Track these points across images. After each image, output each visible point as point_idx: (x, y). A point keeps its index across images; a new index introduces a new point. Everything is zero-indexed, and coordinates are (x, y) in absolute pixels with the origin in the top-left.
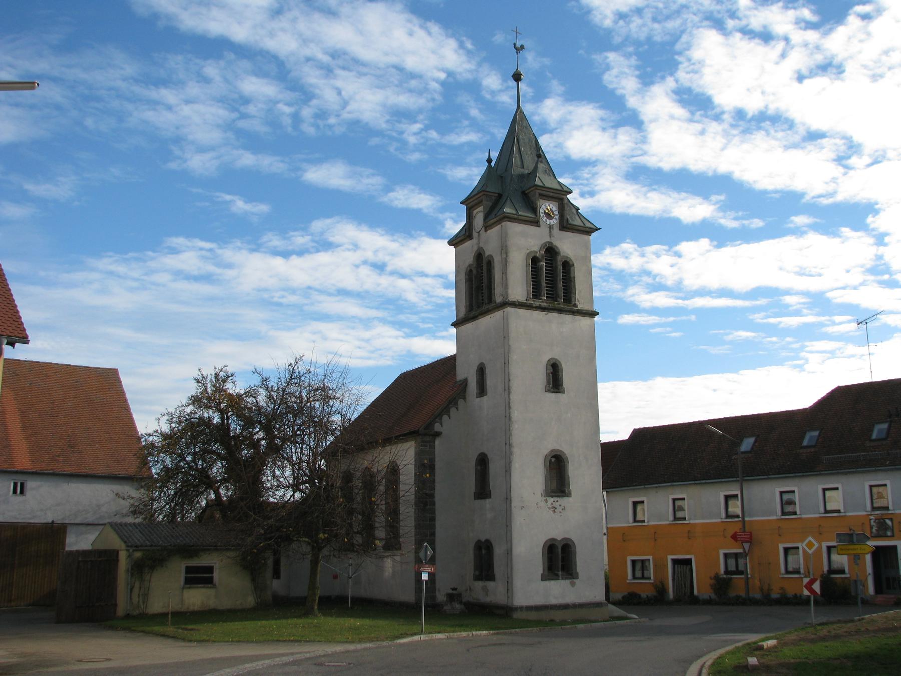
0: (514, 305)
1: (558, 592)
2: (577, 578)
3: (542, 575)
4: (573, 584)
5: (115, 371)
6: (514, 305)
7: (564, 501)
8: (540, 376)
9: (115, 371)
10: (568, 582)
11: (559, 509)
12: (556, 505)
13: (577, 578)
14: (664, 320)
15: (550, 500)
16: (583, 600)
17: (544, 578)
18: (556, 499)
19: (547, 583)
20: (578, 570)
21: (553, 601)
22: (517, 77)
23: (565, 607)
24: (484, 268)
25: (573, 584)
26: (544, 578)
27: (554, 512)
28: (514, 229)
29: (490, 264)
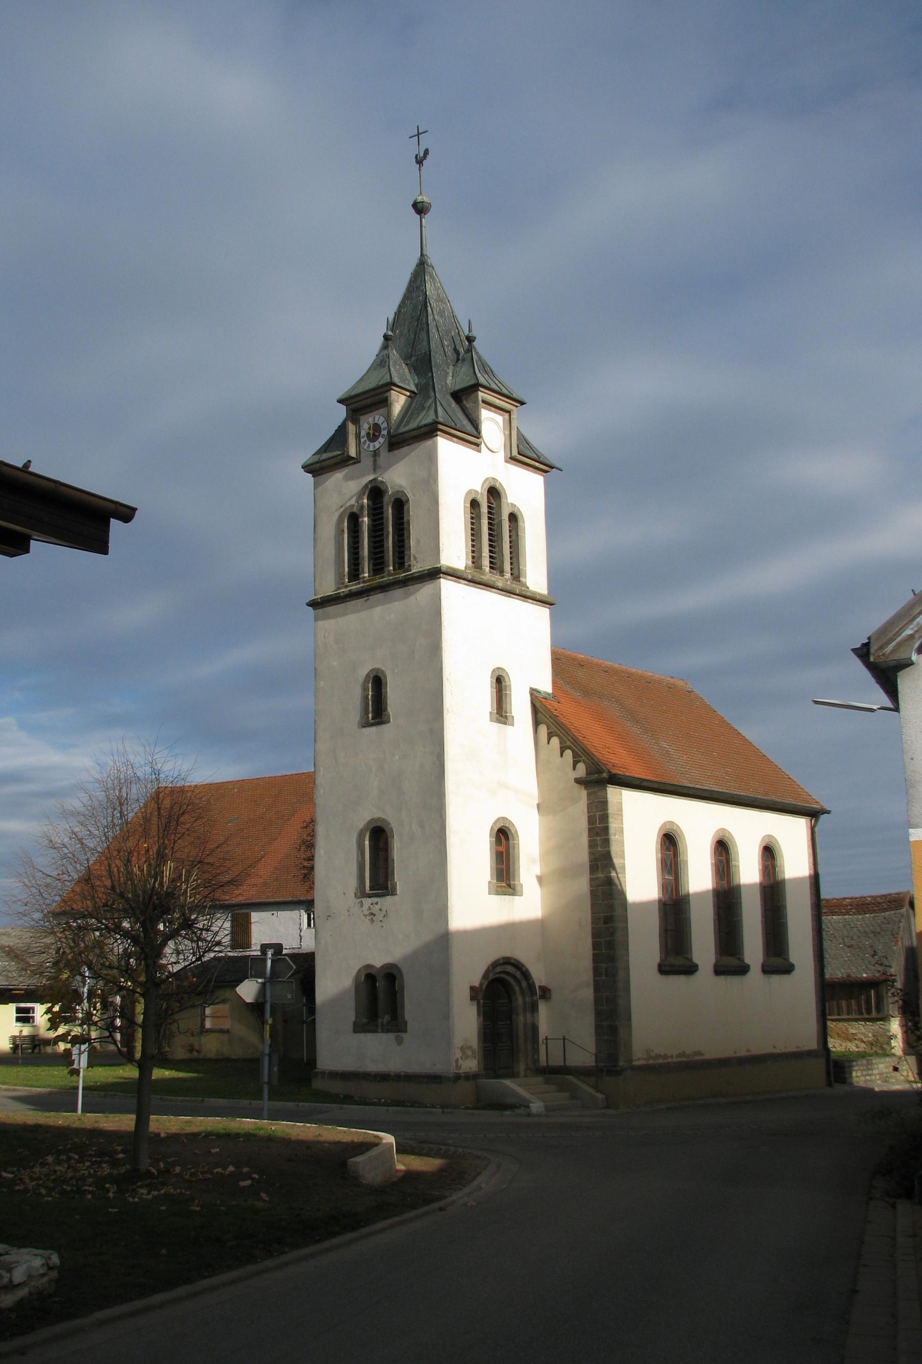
0: (454, 575)
1: (376, 1052)
2: (405, 1031)
3: (355, 1023)
4: (400, 1041)
5: (28, 552)
6: (454, 575)
7: (387, 902)
8: (353, 699)
9: (28, 552)
10: (392, 1036)
11: (380, 916)
12: (375, 909)
13: (405, 1031)
14: (900, 638)
15: (367, 902)
16: (415, 1069)
17: (359, 1028)
18: (375, 900)
19: (361, 1036)
20: (407, 1017)
21: (371, 1067)
22: (420, 209)
23: (383, 1077)
24: (389, 512)
25: (400, 1041)
26: (359, 1028)
27: (372, 921)
28: (446, 448)
29: (400, 505)
